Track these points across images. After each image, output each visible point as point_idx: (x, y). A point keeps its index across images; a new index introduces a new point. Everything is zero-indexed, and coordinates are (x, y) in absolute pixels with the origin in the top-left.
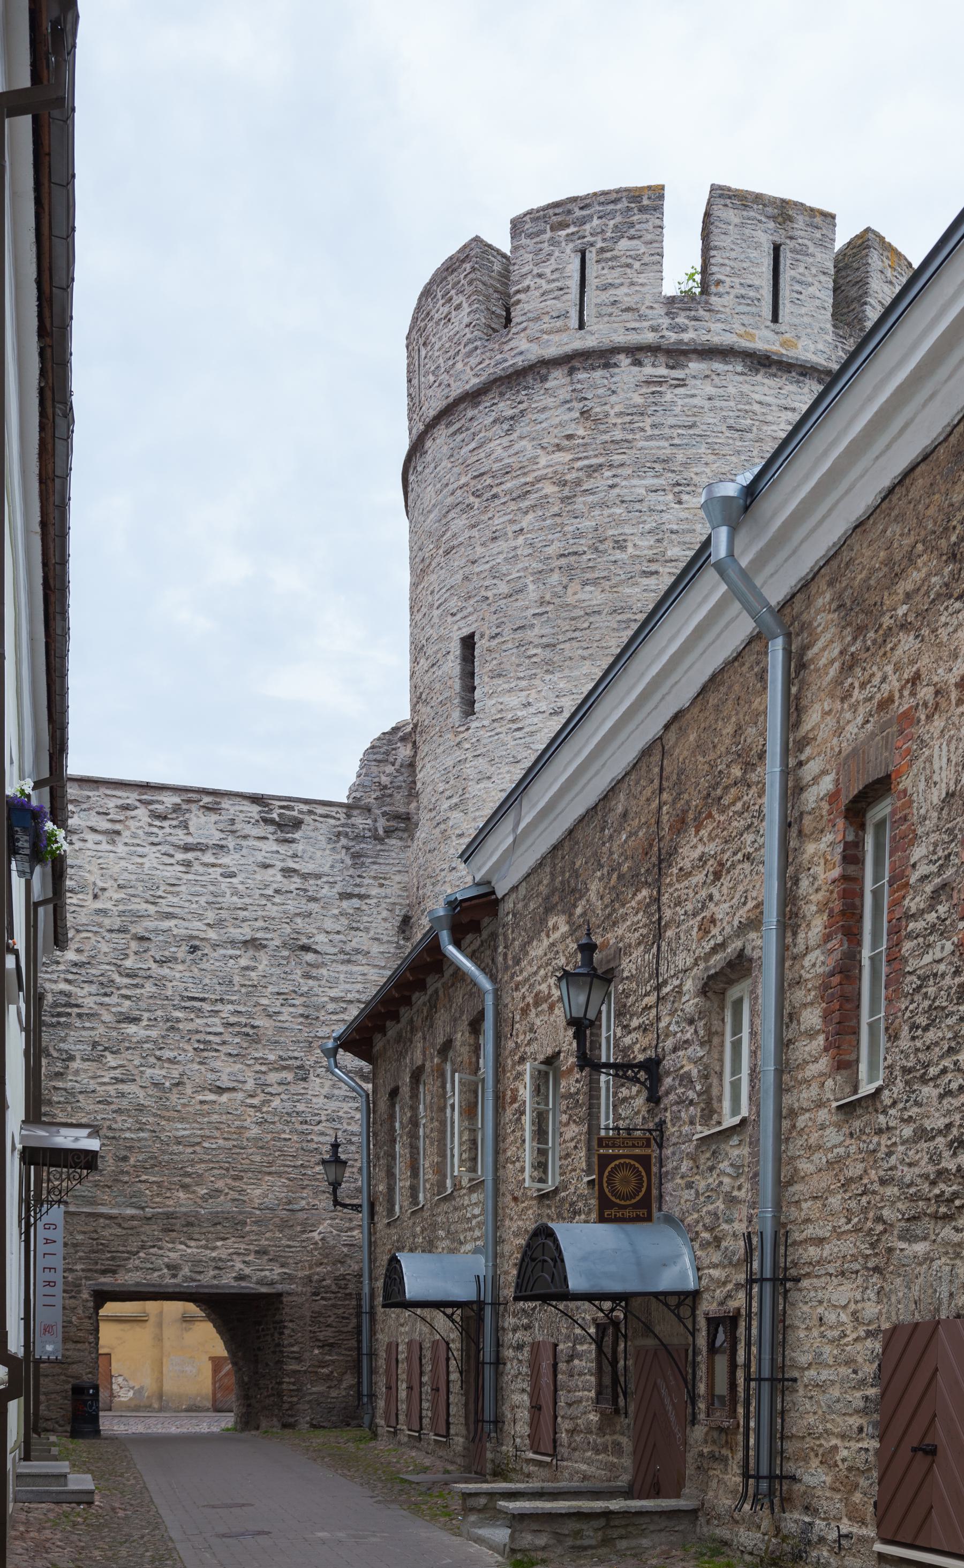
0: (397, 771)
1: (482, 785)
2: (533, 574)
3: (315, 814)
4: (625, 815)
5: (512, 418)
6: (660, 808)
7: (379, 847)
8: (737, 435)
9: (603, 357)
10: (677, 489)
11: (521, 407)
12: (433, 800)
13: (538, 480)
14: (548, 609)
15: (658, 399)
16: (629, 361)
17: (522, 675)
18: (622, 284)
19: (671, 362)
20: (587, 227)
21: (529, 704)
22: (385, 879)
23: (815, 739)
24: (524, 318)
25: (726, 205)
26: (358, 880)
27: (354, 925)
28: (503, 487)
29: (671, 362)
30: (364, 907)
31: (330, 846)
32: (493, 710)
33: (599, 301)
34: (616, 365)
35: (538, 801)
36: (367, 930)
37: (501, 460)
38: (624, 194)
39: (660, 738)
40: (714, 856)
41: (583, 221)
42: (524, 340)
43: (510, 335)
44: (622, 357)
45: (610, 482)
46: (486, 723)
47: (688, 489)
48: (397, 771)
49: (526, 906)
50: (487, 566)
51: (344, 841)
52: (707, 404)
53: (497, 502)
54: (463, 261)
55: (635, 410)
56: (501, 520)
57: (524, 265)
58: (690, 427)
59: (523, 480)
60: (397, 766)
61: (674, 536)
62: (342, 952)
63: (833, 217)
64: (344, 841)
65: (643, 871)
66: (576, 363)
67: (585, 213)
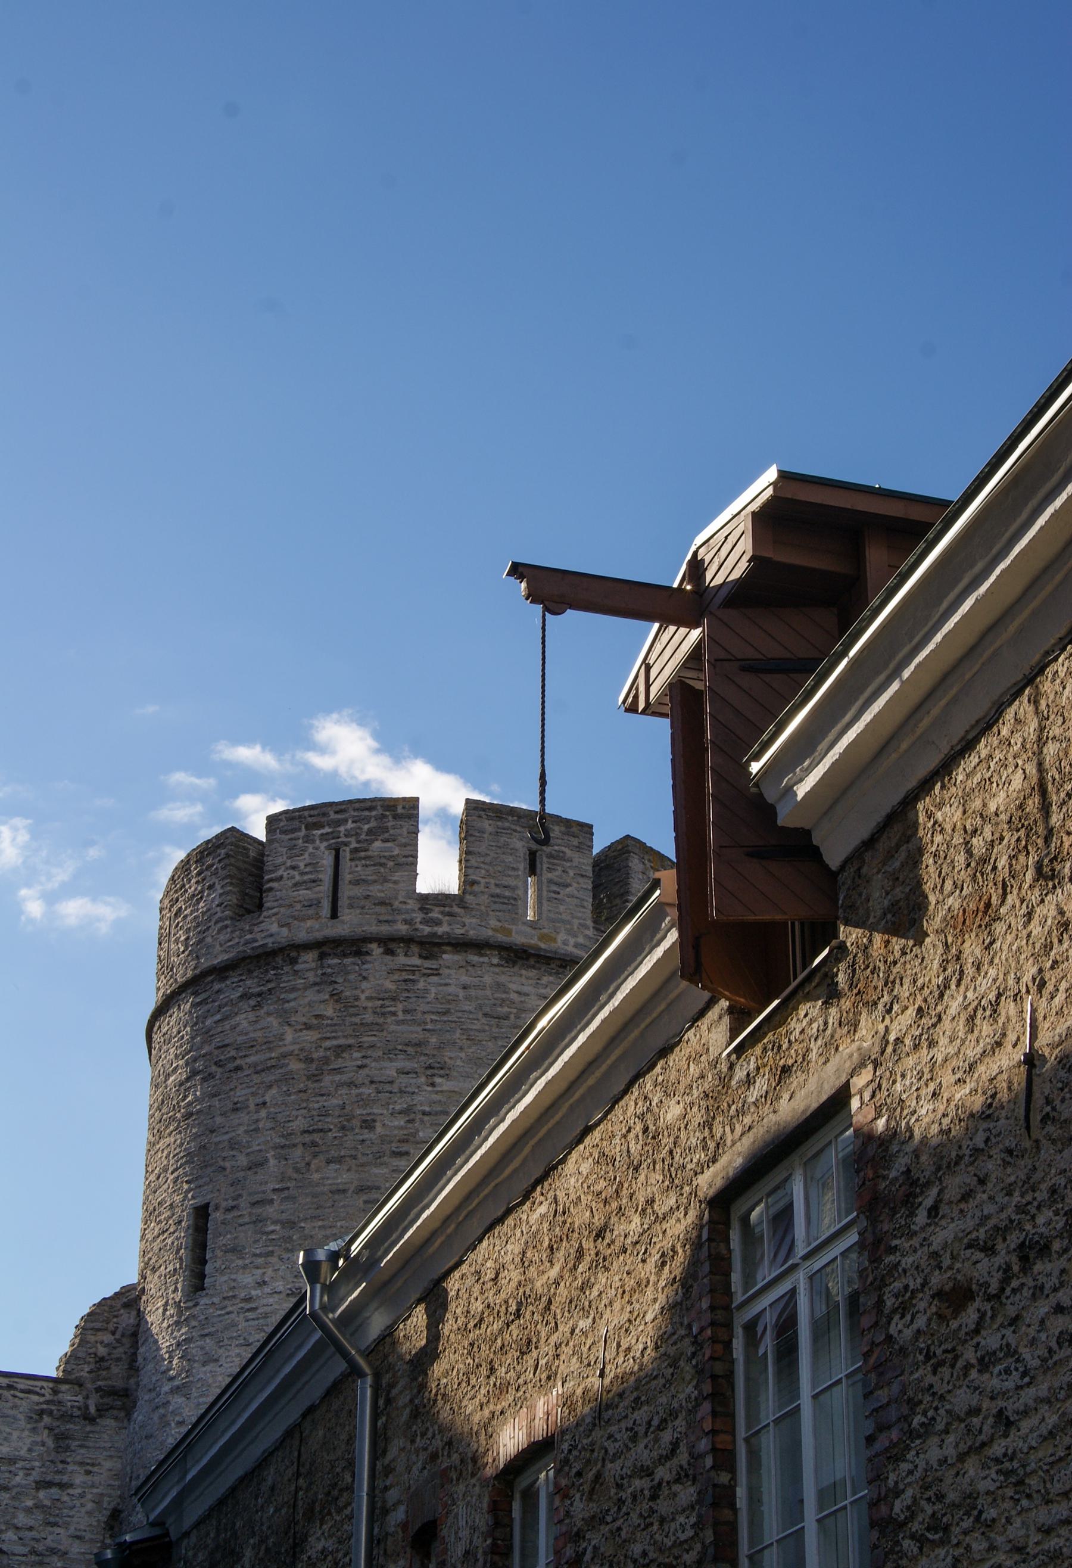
0: (118, 1341)
1: (207, 1368)
2: (275, 1148)
3: (16, 1389)
4: (272, 1488)
5: (260, 995)
6: (296, 1492)
7: (88, 1428)
8: (494, 1022)
9: (354, 946)
10: (429, 1072)
11: (270, 985)
12: (154, 1379)
13: (284, 1056)
14: (289, 1184)
15: (410, 986)
16: (381, 950)
17: (258, 1251)
18: (375, 881)
19: (425, 953)
20: (342, 829)
21: (265, 1283)
22: (93, 1465)
23: (394, 1469)
24: (275, 904)
25: (480, 817)
26: (60, 1466)
27: (52, 1519)
28: (248, 1060)
29: (425, 953)
30: (65, 1498)
31: (29, 1426)
32: (225, 1287)
33: (351, 894)
34: (367, 953)
35: (201, 1458)
36: (66, 1525)
37: (246, 1034)
38: (379, 803)
39: (299, 1425)
40: (331, 1553)
41: (339, 823)
42: (275, 925)
43: (261, 918)
44: (374, 946)
45: (359, 1063)
46: (216, 1300)
47: (442, 1072)
48: (118, 1341)
49: (195, 1555)
50: (226, 1137)
51: (47, 1419)
52: (461, 994)
53: (240, 1074)
54: (218, 847)
55: (387, 995)
56: (243, 1092)
57: (278, 858)
58: (444, 1014)
59: (268, 1055)
60: (117, 1336)
61: (426, 1118)
62: (33, 1552)
63: (591, 827)
64: (47, 1419)
65: (283, 1550)
66: (325, 949)
67: (339, 816)
